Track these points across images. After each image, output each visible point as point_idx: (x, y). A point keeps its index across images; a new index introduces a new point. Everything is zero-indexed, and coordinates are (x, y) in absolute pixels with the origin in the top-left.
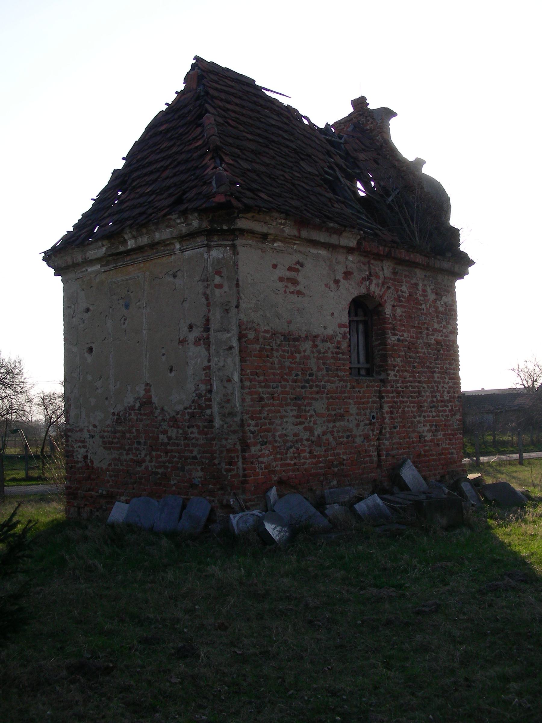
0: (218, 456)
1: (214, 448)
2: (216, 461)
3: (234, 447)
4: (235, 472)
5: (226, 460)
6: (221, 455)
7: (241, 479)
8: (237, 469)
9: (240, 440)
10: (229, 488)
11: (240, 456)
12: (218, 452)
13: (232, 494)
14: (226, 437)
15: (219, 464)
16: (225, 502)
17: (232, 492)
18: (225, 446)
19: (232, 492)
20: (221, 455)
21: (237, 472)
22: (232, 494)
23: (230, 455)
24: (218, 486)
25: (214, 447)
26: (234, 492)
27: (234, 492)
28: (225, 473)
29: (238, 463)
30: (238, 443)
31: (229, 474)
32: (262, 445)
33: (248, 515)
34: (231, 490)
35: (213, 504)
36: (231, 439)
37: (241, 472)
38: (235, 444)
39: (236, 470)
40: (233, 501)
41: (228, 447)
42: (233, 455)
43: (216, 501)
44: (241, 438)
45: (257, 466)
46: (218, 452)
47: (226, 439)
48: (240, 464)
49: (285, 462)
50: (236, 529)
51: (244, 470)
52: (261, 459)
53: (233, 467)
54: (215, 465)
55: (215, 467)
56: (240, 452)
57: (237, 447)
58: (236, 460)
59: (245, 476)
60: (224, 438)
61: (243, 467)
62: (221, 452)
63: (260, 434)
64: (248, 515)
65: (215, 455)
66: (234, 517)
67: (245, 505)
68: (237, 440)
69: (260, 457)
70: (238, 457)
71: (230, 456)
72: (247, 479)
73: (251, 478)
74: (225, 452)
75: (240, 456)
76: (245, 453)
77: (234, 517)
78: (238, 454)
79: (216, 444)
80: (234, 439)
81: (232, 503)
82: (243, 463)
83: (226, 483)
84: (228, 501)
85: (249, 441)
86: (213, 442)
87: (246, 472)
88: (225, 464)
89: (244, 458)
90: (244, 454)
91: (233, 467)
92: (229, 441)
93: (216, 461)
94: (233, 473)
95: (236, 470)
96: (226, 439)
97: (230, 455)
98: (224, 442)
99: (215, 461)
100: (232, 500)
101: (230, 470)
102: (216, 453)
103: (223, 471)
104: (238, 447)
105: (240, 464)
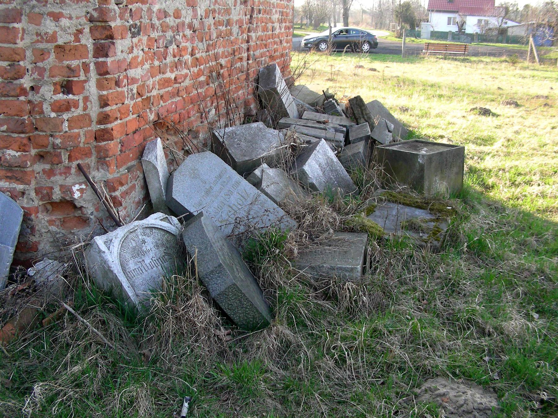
0: (29, 67)
1: (20, 44)
2: (26, 82)
3: (77, 40)
4: (79, 111)
5: (57, 79)
6: (40, 64)
7: (95, 127)
8: (85, 104)
9: (91, 20)
10: (65, 157)
11: (92, 66)
12: (29, 53)
13: (73, 171)
14: (57, 10)
15: (32, 88)
16: (57, 195)
17: (74, 164)
18: (53, 38)
19: (74, 164)
20: (40, 64)
21: (85, 109)
22: (73, 171)
23: (66, 63)
24: (33, 152)
25: (18, 41)
26: (79, 165)
27: (79, 165)
28: (53, 115)
29: (86, 85)
30: (87, 30)
31: (65, 116)
32: (134, 35)
33: (139, 231)
34: (70, 158)
35: (25, 202)
36: (70, 18)
37: (94, 111)
38: (80, 32)
39: (81, 104)
40: (81, 191)
41: (60, 42)
42: (74, 63)
43: (33, 194)
44: (95, 14)
45: (125, 89)
46: (29, 53)
47: (56, 17)
48: (92, 88)
49: (164, 76)
50: (130, 293)
51: (104, 102)
52: (132, 73)
53: (76, 98)
54: (23, 92)
55: (22, 98)
56: (91, 55)
57: (83, 42)
58: (82, 78)
59: (104, 119)
60: (51, 14)
61: (101, 97)
62: (42, 55)
63: (130, 7)
64: (139, 231)
65: (21, 63)
66: (108, 243)
67: (111, 196)
68: (83, 20)
69: (130, 66)
70: (86, 67)
71: (69, 67)
72: (109, 126)
73: (116, 123)
74: (53, 56)
75: (92, 66)
76: (107, 56)
77: (108, 243)
78: (87, 61)
79: (23, 30)
80: (77, 18)
81: (77, 195)
82: (100, 86)
83: (58, 141)
84: (66, 189)
85: (113, 24)
86: (16, 25)
87: (108, 109)
88: (52, 88)
89: (103, 71)
90: (101, 59)
91: (76, 98)
92: (64, 22)
93: (26, 82)
94: (75, 114)
95: (81, 104)
96: (56, 17)
97: (66, 63)
98: (49, 26)
99: (22, 81)
100: (77, 187)
101: (67, 107)
102: (24, 58)
103: (46, 107)
104: (87, 41)
105: (92, 88)
